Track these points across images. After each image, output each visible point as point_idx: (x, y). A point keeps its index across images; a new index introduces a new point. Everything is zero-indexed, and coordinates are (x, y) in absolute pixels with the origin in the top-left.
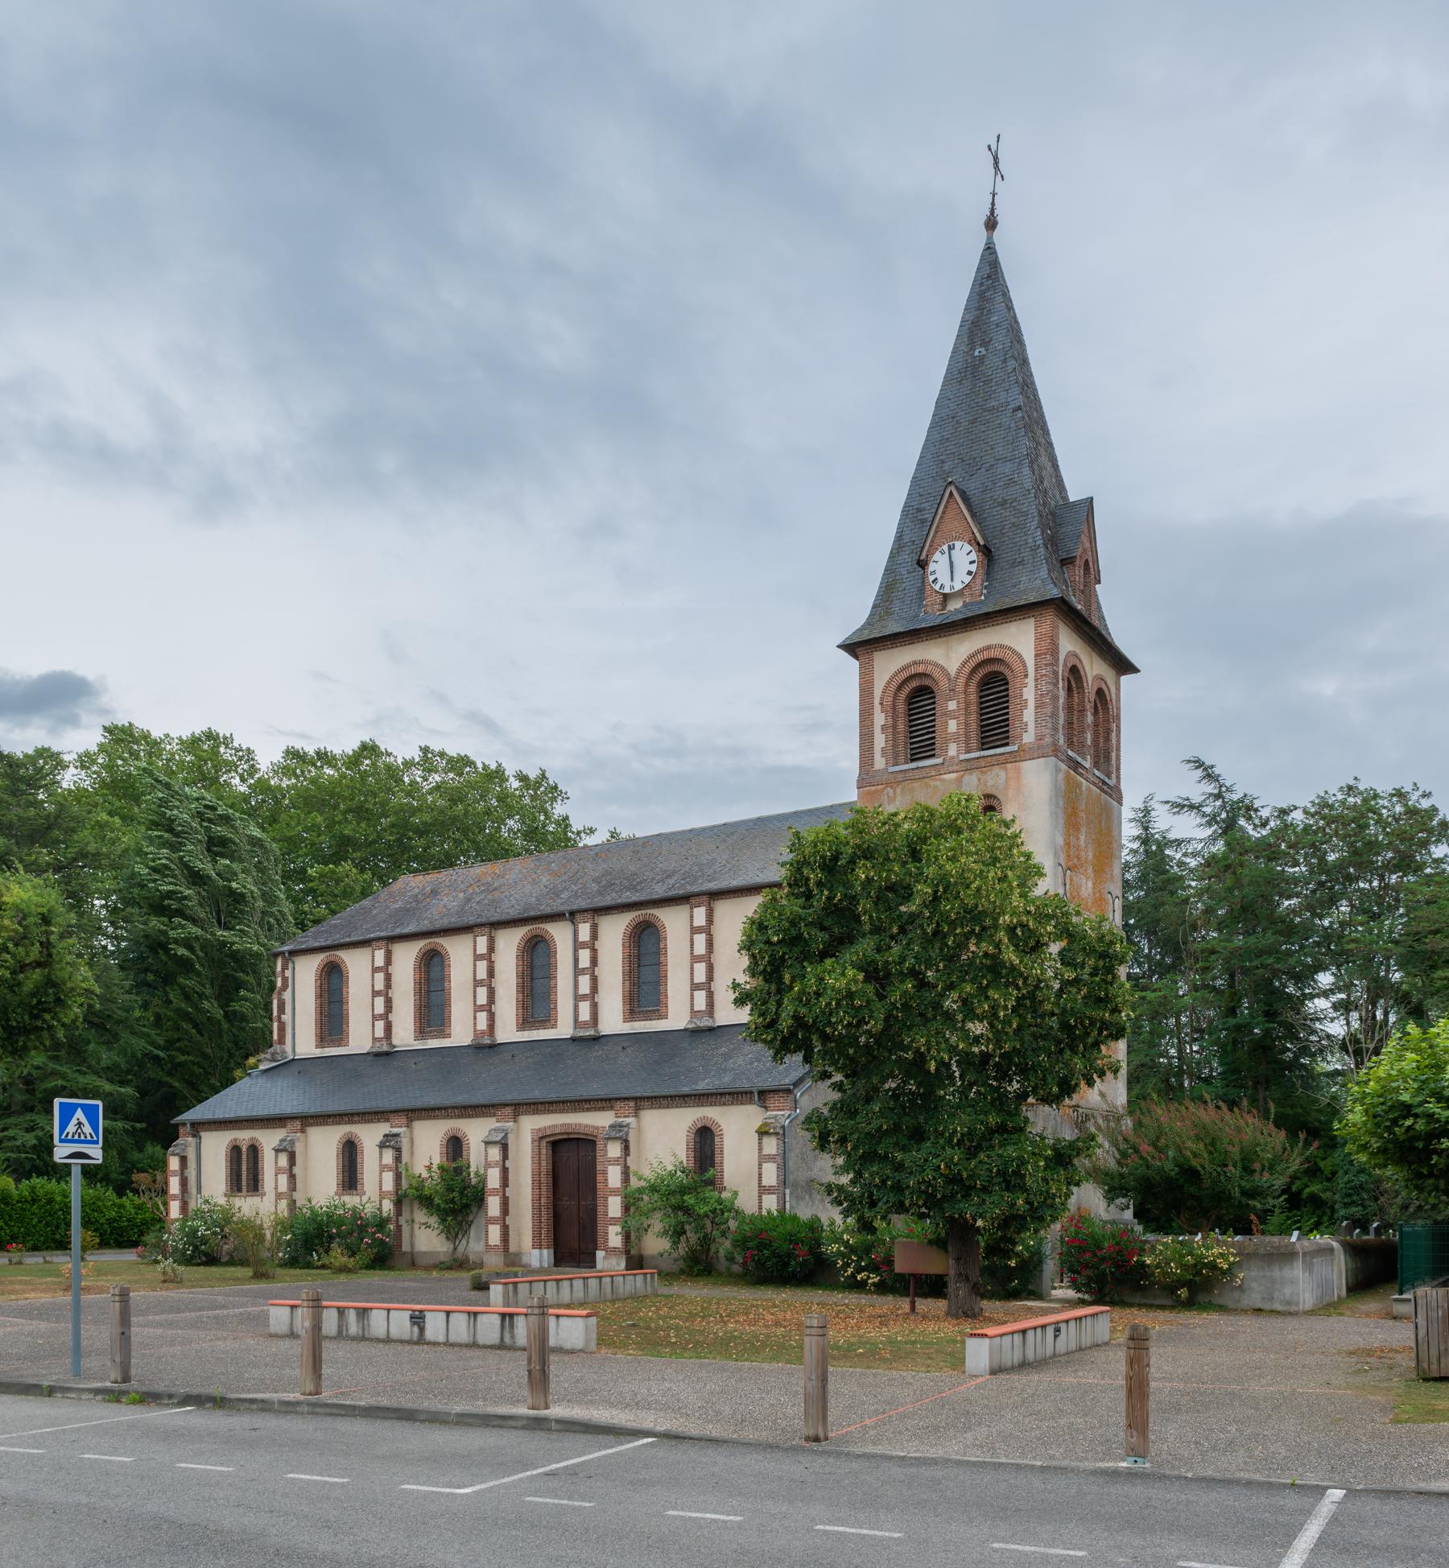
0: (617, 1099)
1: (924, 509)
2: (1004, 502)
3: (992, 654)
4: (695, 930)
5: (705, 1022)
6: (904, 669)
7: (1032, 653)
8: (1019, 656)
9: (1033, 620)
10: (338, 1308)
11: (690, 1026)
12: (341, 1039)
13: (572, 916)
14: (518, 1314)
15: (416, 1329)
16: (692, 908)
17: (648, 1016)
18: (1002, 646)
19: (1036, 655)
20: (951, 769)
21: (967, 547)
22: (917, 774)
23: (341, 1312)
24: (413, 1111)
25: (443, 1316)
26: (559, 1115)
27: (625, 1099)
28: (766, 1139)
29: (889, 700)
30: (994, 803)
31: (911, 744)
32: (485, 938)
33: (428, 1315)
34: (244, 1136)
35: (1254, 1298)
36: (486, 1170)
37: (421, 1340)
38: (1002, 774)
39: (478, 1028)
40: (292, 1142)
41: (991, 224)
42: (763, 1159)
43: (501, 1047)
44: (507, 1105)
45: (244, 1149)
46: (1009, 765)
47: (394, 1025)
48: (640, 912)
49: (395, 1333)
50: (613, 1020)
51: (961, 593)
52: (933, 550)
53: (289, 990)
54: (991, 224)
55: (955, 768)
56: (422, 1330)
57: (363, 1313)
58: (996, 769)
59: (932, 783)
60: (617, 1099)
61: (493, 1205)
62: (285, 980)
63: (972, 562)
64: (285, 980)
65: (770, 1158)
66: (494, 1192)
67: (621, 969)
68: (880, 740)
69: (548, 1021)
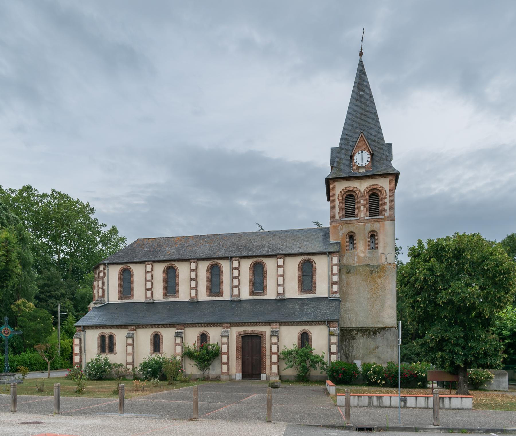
0: (272, 322)
1: (348, 139)
2: (375, 141)
3: (375, 187)
4: (278, 266)
5: (282, 297)
6: (346, 188)
7: (388, 189)
8: (384, 189)
9: (388, 178)
10: (369, 396)
11: (277, 298)
12: (130, 297)
13: (231, 259)
14: (445, 397)
15: (403, 403)
16: (278, 259)
17: (259, 294)
18: (378, 185)
19: (389, 189)
20: (362, 221)
21: (367, 153)
22: (350, 222)
23: (370, 397)
24: (137, 325)
25: (415, 398)
26: (247, 327)
27: (275, 322)
28: (128, 339)
29: (340, 198)
30: (375, 233)
31: (346, 212)
32: (237, 262)
33: (408, 398)
34: (107, 332)
35: (494, 387)
36: (222, 346)
37: (405, 407)
38: (379, 225)
39: (192, 295)
40: (133, 334)
41: (361, 54)
42: (176, 344)
43: (200, 303)
44: (228, 323)
45: (107, 336)
46: (381, 222)
47: (154, 292)
48: (256, 259)
49: (393, 404)
50: (245, 294)
51: (365, 167)
52: (355, 153)
53: (106, 277)
54: (361, 54)
55: (363, 221)
56: (405, 403)
57: (379, 398)
58: (376, 223)
59: (355, 225)
60: (272, 322)
61: (225, 358)
62: (104, 274)
63: (368, 158)
64: (104, 274)
65: (179, 344)
66: (225, 353)
67: (249, 277)
68: (337, 210)
69: (220, 293)
